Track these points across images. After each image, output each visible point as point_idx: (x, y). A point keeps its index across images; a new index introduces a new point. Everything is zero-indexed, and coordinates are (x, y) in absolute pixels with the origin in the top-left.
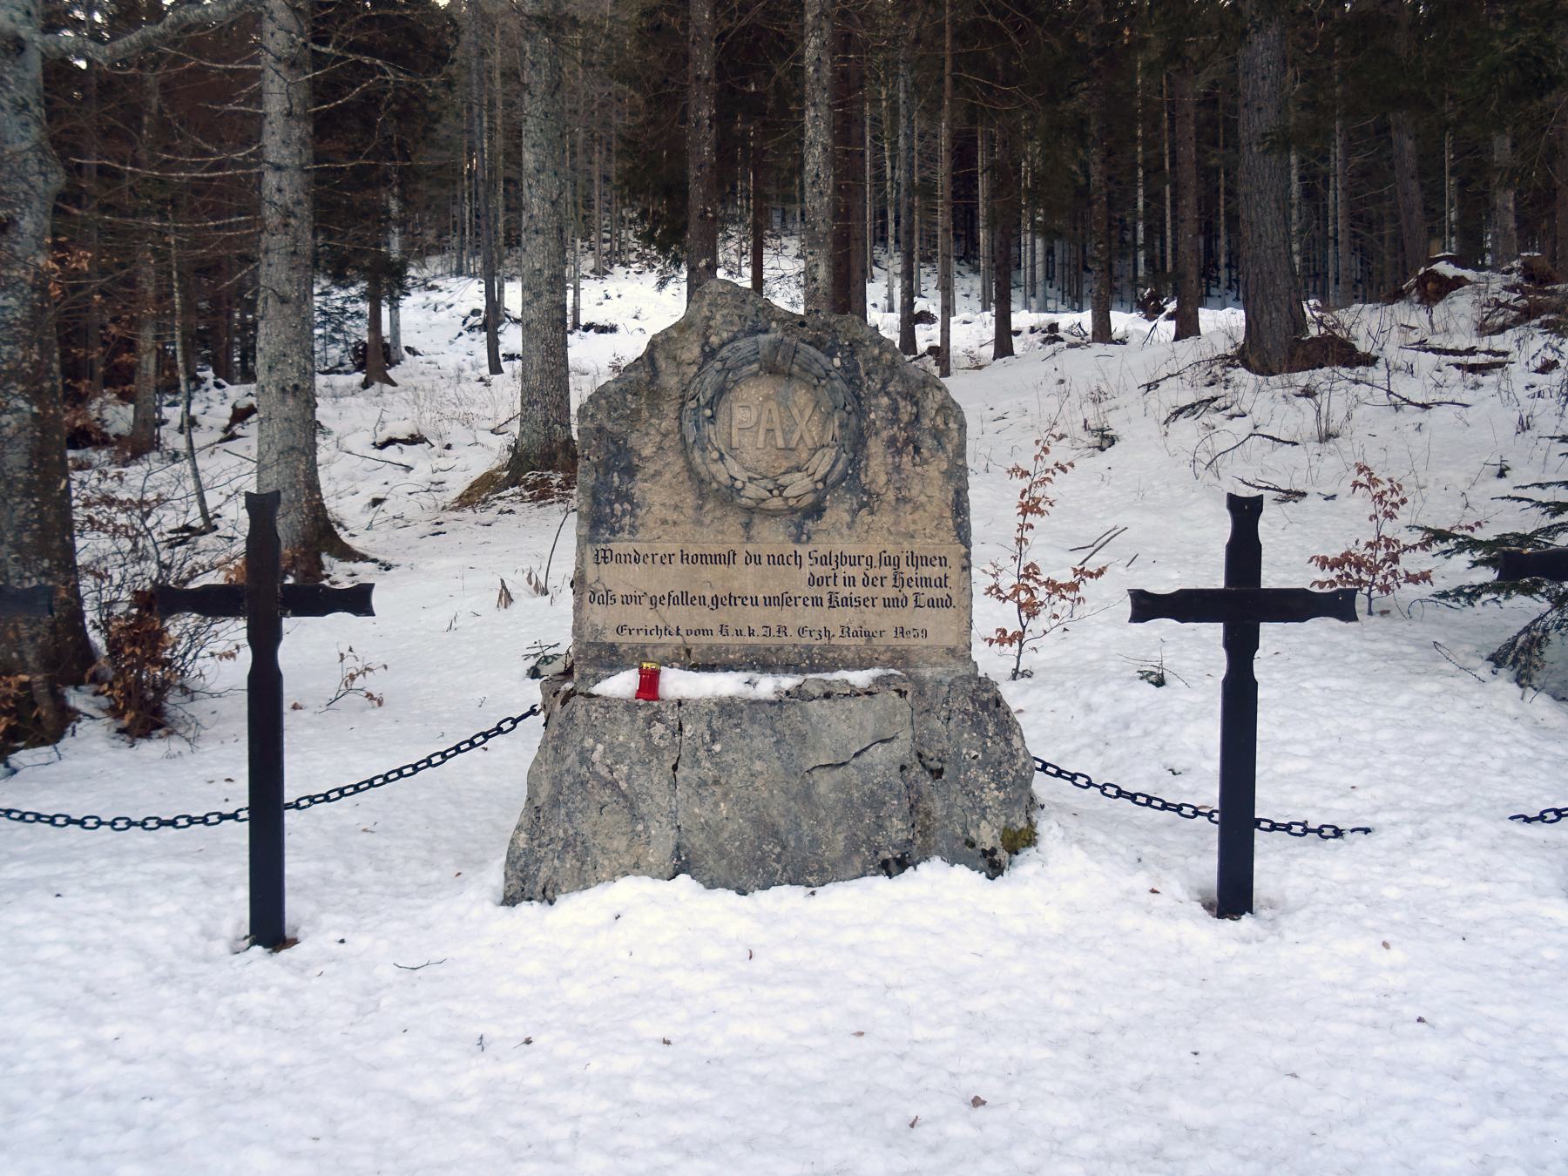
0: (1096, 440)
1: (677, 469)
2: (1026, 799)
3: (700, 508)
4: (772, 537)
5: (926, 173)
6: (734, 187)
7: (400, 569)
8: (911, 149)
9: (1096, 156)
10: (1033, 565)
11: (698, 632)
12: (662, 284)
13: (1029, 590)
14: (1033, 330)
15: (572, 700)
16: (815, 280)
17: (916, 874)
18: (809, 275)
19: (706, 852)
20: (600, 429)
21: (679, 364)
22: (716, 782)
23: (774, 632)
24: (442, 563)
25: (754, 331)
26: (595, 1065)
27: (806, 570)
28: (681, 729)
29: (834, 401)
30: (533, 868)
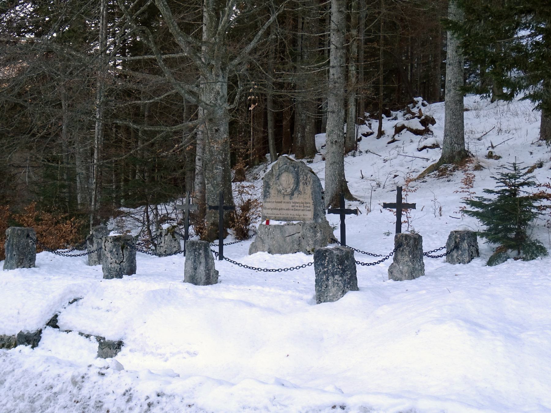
4: (287, 199)
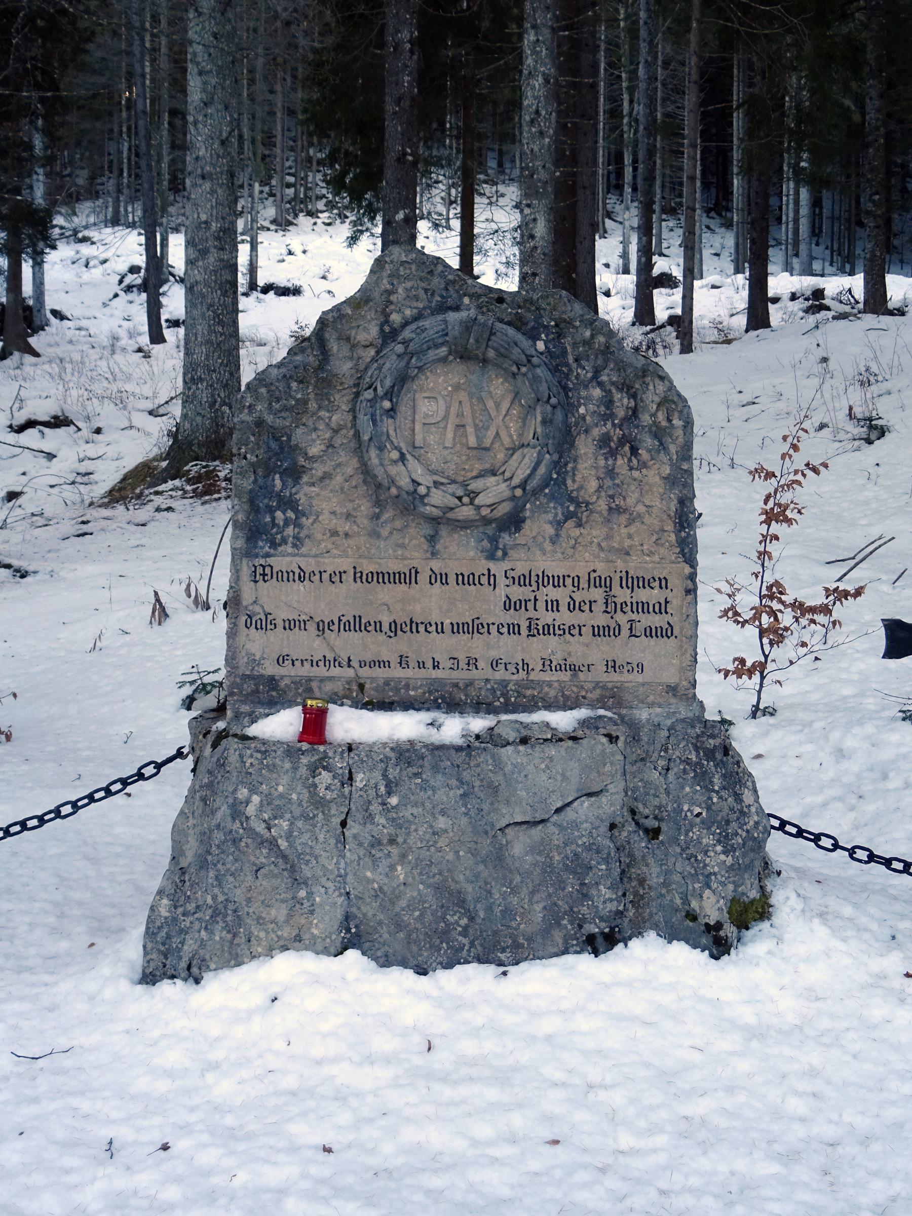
0: (863, 431)
1: (349, 470)
2: (758, 864)
3: (377, 517)
4: (462, 552)
5: (671, 108)
6: (442, 124)
7: (38, 577)
8: (653, 78)
9: (872, 87)
10: (777, 584)
11: (373, 664)
12: (353, 240)
13: (773, 613)
14: (793, 297)
15: (224, 742)
16: (532, 237)
17: (626, 952)
18: (525, 233)
19: (380, 923)
20: (260, 423)
21: (353, 347)
22: (392, 841)
23: (463, 665)
24: (90, 569)
25: (443, 308)
26: (242, 1177)
27: (502, 591)
28: (351, 778)
29: (536, 392)
30: (176, 941)
